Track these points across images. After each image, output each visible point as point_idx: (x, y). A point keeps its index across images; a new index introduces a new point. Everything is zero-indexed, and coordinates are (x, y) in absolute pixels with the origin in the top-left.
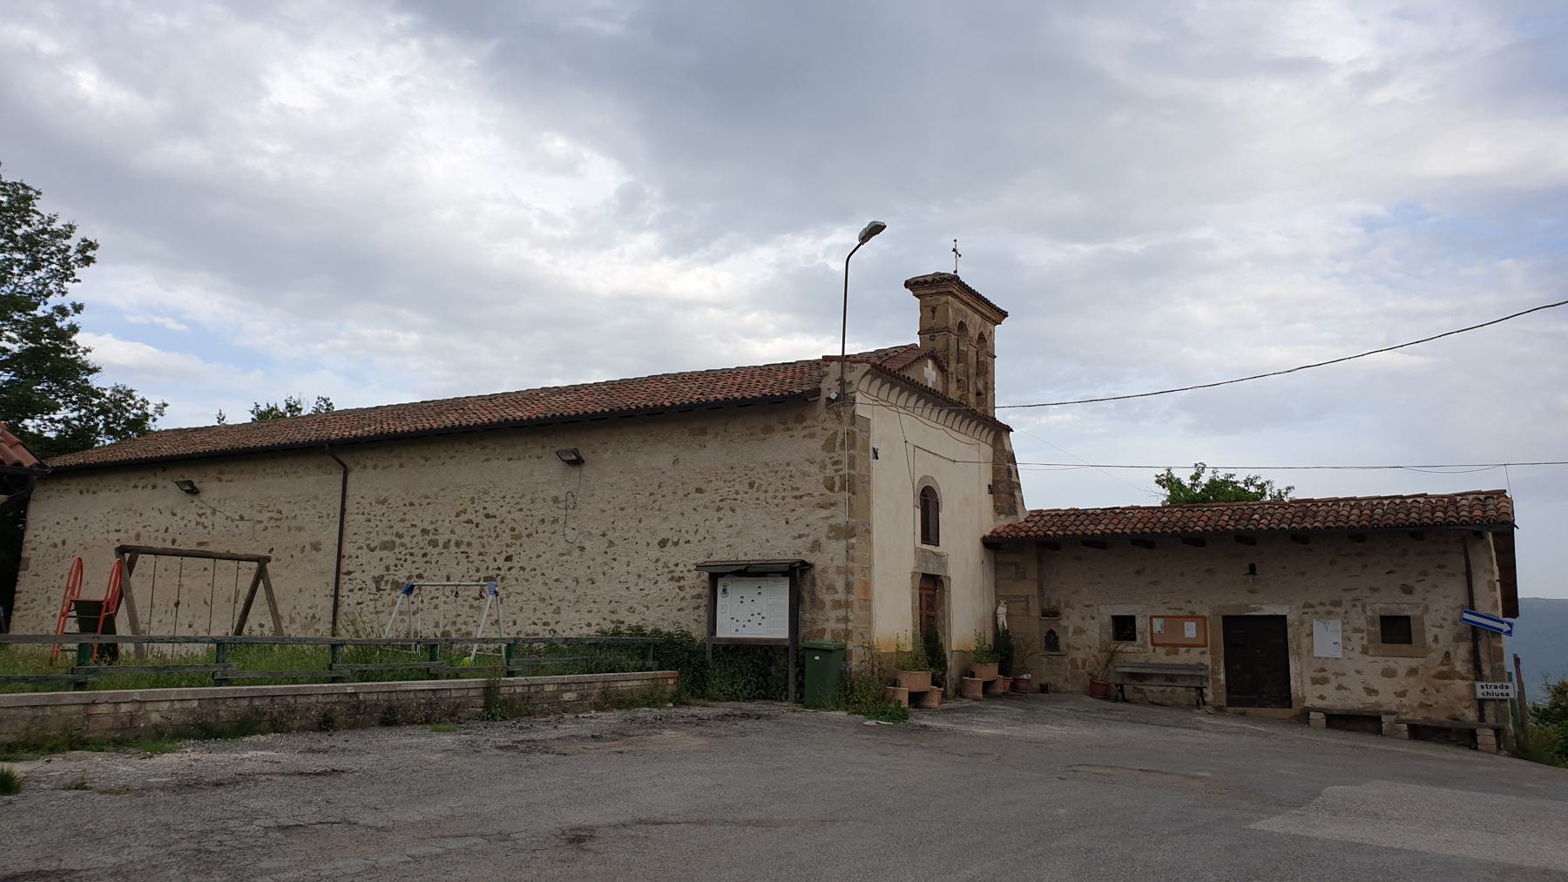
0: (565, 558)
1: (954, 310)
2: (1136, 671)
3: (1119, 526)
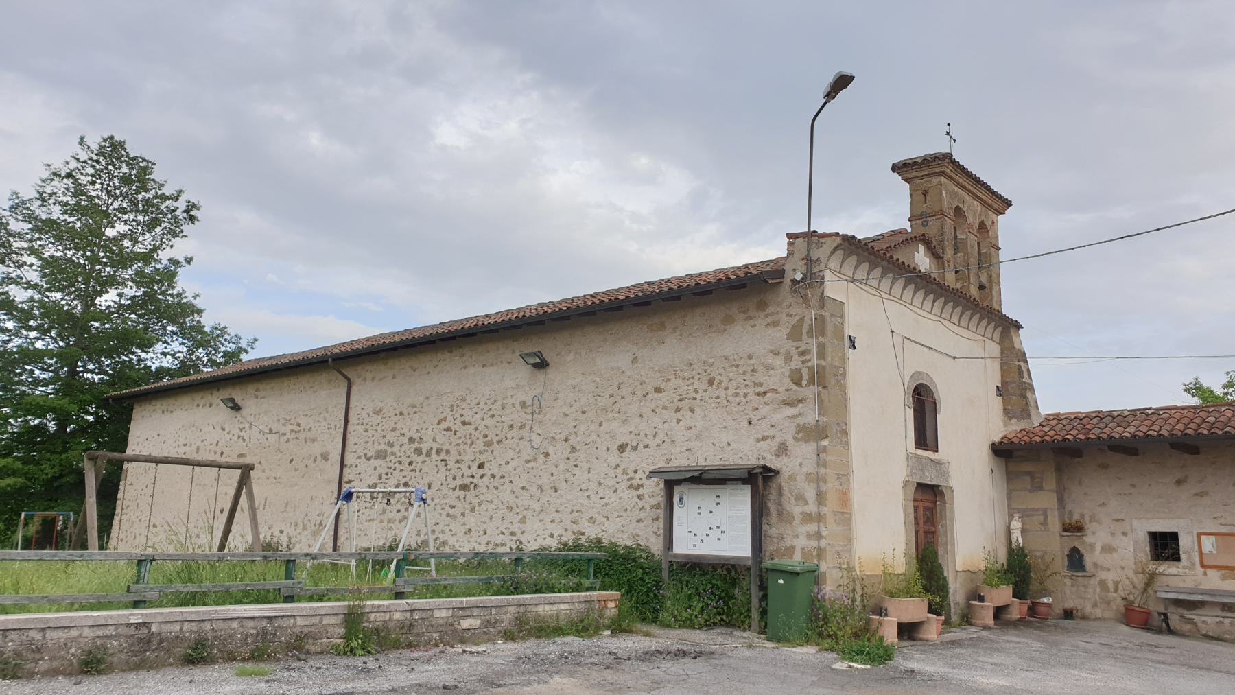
0: (530, 465)
1: (947, 193)
2: (1181, 597)
3: (1153, 428)
